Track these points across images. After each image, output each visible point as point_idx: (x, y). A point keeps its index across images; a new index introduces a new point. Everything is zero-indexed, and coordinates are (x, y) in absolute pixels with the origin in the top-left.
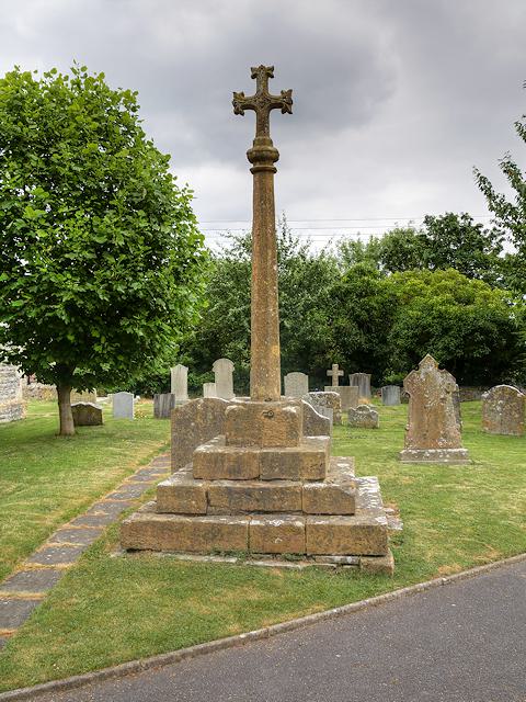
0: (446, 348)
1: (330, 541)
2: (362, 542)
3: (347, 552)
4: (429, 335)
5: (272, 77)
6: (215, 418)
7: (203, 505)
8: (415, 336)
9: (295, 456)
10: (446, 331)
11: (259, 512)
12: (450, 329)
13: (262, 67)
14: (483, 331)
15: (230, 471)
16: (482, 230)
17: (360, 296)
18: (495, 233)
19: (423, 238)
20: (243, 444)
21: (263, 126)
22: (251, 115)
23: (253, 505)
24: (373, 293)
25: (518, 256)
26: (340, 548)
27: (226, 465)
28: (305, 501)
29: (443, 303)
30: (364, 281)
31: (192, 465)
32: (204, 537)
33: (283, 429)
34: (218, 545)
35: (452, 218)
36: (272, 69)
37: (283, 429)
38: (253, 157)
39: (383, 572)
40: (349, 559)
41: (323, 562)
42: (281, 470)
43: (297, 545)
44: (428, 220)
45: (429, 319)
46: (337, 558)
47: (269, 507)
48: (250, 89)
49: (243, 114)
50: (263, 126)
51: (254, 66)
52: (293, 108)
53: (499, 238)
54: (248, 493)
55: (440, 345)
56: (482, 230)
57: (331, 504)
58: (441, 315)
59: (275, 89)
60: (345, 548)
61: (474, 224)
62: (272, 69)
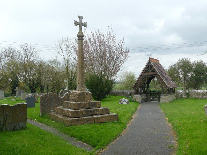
21: (81, 29)
23: (91, 114)
37: (89, 97)
43: (103, 121)
48: (78, 21)
50: (81, 29)
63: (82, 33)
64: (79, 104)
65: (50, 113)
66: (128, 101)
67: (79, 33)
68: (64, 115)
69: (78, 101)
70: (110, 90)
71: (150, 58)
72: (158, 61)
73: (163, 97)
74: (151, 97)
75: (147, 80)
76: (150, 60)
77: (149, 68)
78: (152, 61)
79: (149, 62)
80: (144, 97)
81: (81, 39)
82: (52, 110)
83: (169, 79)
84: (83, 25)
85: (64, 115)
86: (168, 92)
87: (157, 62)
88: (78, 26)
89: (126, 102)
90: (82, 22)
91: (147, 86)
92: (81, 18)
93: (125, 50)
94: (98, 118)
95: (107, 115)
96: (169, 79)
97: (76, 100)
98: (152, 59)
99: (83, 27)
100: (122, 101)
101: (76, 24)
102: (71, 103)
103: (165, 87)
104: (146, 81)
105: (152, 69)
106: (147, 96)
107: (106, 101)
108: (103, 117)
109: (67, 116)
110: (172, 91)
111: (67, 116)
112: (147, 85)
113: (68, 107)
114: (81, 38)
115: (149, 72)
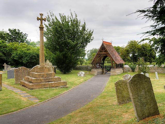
0: (27, 60)
4: (22, 57)
6: (23, 70)
7: (40, 81)
8: (19, 57)
9: (51, 74)
10: (27, 56)
11: (48, 82)
12: (27, 56)
14: (34, 56)
15: (42, 76)
16: (22, 33)
17: (4, 47)
18: (26, 34)
19: (8, 34)
20: (42, 73)
21: (42, 23)
23: (48, 81)
24: (7, 47)
25: (44, 42)
28: (56, 80)
29: (25, 50)
30: (4, 44)
33: (47, 70)
34: (45, 87)
35: (15, 30)
37: (47, 70)
38: (40, 28)
39: (67, 87)
40: (63, 86)
41: (59, 87)
43: (56, 85)
44: (9, 30)
45: (22, 53)
46: (61, 87)
47: (50, 81)
48: (40, 17)
50: (42, 23)
53: (27, 36)
54: (47, 79)
55: (25, 59)
56: (22, 33)
58: (25, 53)
61: (20, 32)
63: (43, 25)
64: (40, 75)
65: (21, 81)
66: (84, 73)
67: (40, 25)
68: (30, 82)
69: (39, 73)
70: (161, 54)
71: (103, 42)
72: (111, 43)
73: (112, 71)
74: (106, 71)
75: (102, 58)
76: (104, 43)
77: (103, 49)
78: (105, 44)
79: (103, 44)
80: (100, 70)
81: (42, 30)
82: (23, 79)
83: (118, 57)
84: (43, 20)
85: (30, 82)
86: (117, 66)
87: (109, 44)
88: (39, 20)
89: (83, 74)
90: (42, 18)
91: (102, 62)
92: (41, 15)
93: (89, 31)
94: (52, 84)
95: (59, 82)
96: (118, 57)
97: (38, 71)
98: (105, 42)
99: (43, 21)
100: (81, 73)
101: (38, 19)
102: (34, 74)
103: (114, 63)
104: (102, 59)
105: (105, 50)
106: (102, 70)
107: (72, 73)
108: (56, 83)
109: (31, 82)
110: (121, 66)
111: (31, 82)
112: (103, 61)
113: (33, 76)
114: (42, 29)
115: (102, 52)
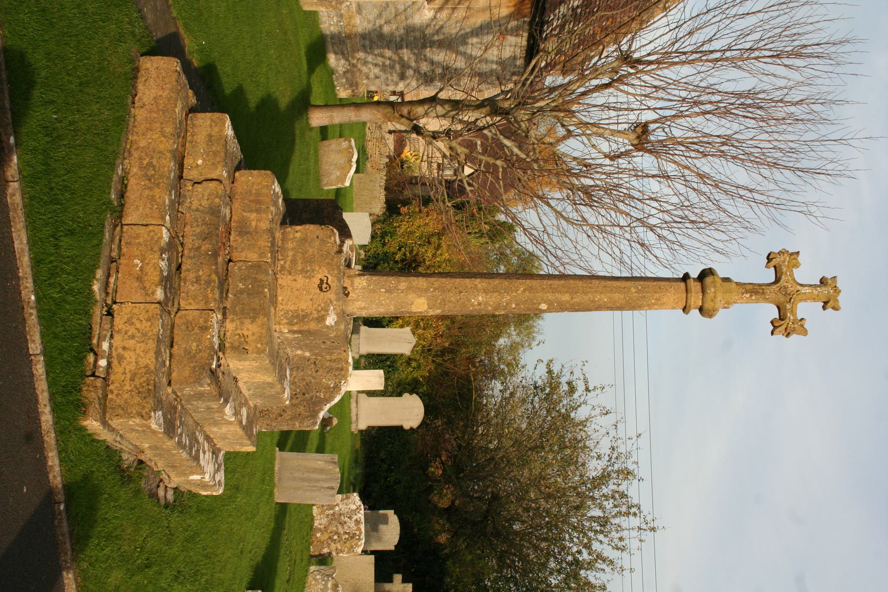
1: (133, 337)
2: (127, 383)
3: (115, 362)
5: (824, 308)
13: (837, 291)
21: (755, 291)
22: (769, 276)
26: (120, 351)
27: (254, 216)
31: (332, 308)
32: (150, 164)
36: (836, 308)
42: (241, 292)
49: (767, 267)
50: (755, 291)
51: (838, 279)
52: (779, 337)
57: (187, 351)
59: (808, 310)
60: (121, 358)
62: (836, 308)
